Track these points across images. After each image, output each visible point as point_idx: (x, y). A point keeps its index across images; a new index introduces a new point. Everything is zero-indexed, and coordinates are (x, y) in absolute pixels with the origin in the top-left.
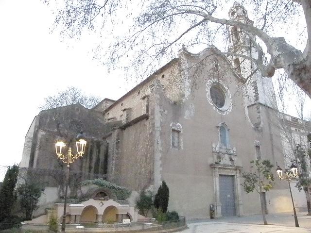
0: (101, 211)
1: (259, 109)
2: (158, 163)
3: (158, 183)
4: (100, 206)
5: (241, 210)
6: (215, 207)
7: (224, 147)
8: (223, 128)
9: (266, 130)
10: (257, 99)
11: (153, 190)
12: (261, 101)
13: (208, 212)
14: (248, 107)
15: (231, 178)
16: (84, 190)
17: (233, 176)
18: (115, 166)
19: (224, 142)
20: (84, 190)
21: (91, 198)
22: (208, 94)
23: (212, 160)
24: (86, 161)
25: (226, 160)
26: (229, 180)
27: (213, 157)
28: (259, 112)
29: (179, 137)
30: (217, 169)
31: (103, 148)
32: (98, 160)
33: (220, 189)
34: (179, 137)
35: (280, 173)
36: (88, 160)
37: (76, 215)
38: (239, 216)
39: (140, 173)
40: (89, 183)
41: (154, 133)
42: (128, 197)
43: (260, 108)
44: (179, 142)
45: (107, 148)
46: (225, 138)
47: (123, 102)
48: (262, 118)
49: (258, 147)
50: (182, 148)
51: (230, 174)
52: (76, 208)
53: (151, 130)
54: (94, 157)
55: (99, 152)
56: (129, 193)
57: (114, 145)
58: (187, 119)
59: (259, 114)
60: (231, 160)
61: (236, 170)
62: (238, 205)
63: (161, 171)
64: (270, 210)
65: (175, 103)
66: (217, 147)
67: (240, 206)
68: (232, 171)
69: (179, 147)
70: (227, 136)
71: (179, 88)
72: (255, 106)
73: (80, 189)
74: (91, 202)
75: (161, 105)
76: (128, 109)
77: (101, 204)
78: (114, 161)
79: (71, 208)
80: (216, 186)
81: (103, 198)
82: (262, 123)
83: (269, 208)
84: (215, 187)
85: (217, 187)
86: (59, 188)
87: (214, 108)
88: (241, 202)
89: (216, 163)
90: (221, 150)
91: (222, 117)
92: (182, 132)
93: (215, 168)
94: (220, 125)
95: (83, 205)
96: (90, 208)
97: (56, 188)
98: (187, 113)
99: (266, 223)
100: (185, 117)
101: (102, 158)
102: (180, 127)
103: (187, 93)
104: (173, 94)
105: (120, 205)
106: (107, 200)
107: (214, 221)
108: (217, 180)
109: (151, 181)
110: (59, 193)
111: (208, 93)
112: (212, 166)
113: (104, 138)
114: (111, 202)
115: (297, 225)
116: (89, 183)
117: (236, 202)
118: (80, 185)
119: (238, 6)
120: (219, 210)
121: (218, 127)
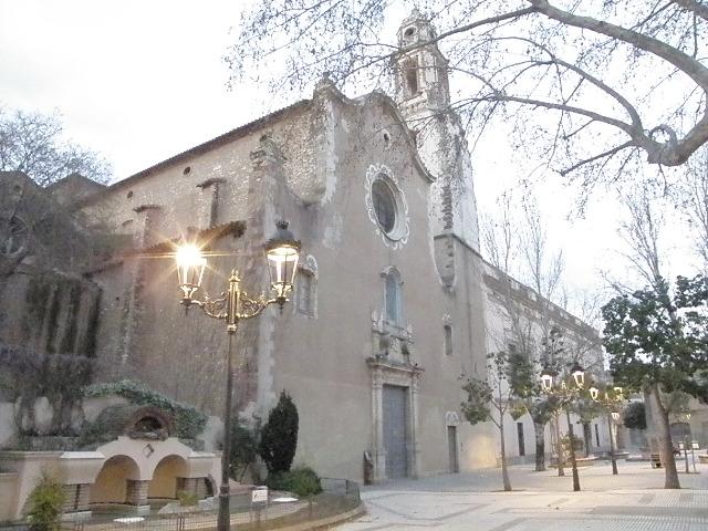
0: (146, 469)
1: (451, 247)
2: (267, 347)
3: (267, 401)
4: (145, 456)
5: (419, 465)
6: (374, 458)
7: (391, 322)
8: (391, 279)
9: (462, 295)
10: (449, 226)
11: (256, 412)
12: (456, 230)
13: (359, 468)
14: (436, 238)
15: (400, 393)
16: (91, 410)
17: (405, 389)
18: (130, 349)
19: (391, 312)
20: (91, 410)
21: (121, 434)
22: (368, 196)
23: (370, 349)
24: (39, 334)
25: (395, 354)
26: (398, 395)
27: (373, 342)
28: (451, 255)
29: (308, 289)
30: (380, 371)
31: (87, 300)
32: (71, 332)
33: (385, 416)
34: (308, 289)
35: (579, 377)
36: (45, 332)
37: (79, 486)
38: (415, 478)
39: (210, 371)
40: (105, 392)
41: (259, 273)
42: (201, 430)
43: (455, 246)
44: (308, 302)
45: (98, 302)
46: (394, 299)
47: (133, 189)
48: (456, 267)
49: (447, 328)
50: (316, 316)
51: (401, 384)
52: (84, 461)
53: (250, 263)
54: (62, 324)
55: (75, 311)
56: (202, 422)
57: (128, 294)
58: (327, 246)
59: (451, 258)
60: (405, 352)
61: (412, 374)
62: (414, 452)
63: (272, 368)
64: (463, 465)
65: (306, 205)
66: (379, 319)
67: (417, 455)
68: (405, 376)
69: (309, 312)
70: (398, 298)
71: (314, 165)
72: (445, 240)
73: (80, 408)
74: (123, 446)
75: (277, 205)
76: (152, 207)
77: (147, 451)
78: (127, 338)
79: (70, 464)
80: (377, 409)
81: (153, 434)
82: (456, 279)
83: (461, 460)
84: (374, 411)
85: (379, 413)
86: (17, 406)
87: (378, 231)
88: (418, 447)
89: (378, 357)
90: (388, 329)
91: (391, 254)
92: (316, 277)
93: (377, 367)
94: (387, 271)
95: (102, 454)
96: (120, 463)
97: (10, 405)
98: (328, 233)
99: (508, 489)
100: (324, 242)
101: (83, 325)
102: (313, 263)
103: (331, 185)
104: (299, 175)
105: (194, 454)
106: (164, 439)
107: (375, 489)
108: (379, 395)
109: (251, 392)
110: (18, 419)
111: (369, 196)
112: (372, 364)
113: (88, 275)
114: (172, 446)
115: (577, 488)
116: (105, 392)
117: (410, 447)
118: (80, 396)
119: (423, 22)
120: (381, 465)
121: (383, 275)
